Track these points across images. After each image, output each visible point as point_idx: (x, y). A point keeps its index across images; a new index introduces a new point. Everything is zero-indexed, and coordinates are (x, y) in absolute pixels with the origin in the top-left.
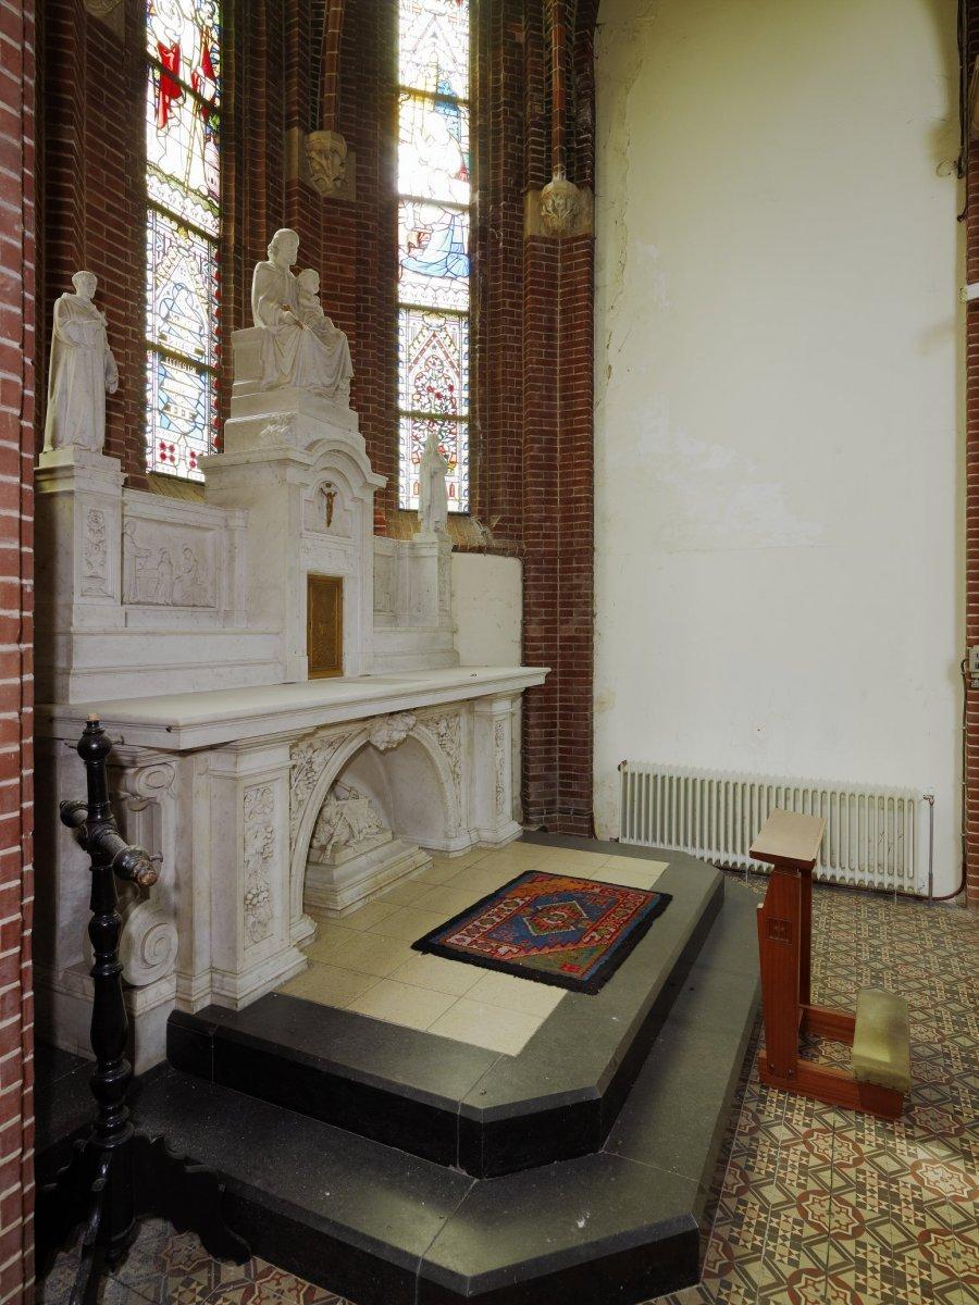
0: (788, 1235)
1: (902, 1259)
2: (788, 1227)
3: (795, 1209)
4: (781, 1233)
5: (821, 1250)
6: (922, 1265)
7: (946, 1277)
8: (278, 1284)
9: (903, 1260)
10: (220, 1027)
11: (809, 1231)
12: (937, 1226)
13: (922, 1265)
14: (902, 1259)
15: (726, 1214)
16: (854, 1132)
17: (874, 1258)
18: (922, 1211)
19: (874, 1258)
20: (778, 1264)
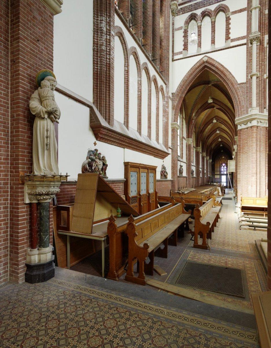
0: (203, 343)
1: (30, 325)
2: (183, 335)
3: (48, 330)
4: (202, 343)
5: (18, 339)
6: (13, 326)
7: (56, 328)
8: (95, 340)
9: (4, 345)
10: (164, 282)
11: (188, 335)
12: (19, 334)
13: (8, 341)
14: (30, 325)
15: (196, 341)
16: (197, 345)
17: (46, 339)
18: (25, 333)
19: (46, 339)
20: (179, 344)
